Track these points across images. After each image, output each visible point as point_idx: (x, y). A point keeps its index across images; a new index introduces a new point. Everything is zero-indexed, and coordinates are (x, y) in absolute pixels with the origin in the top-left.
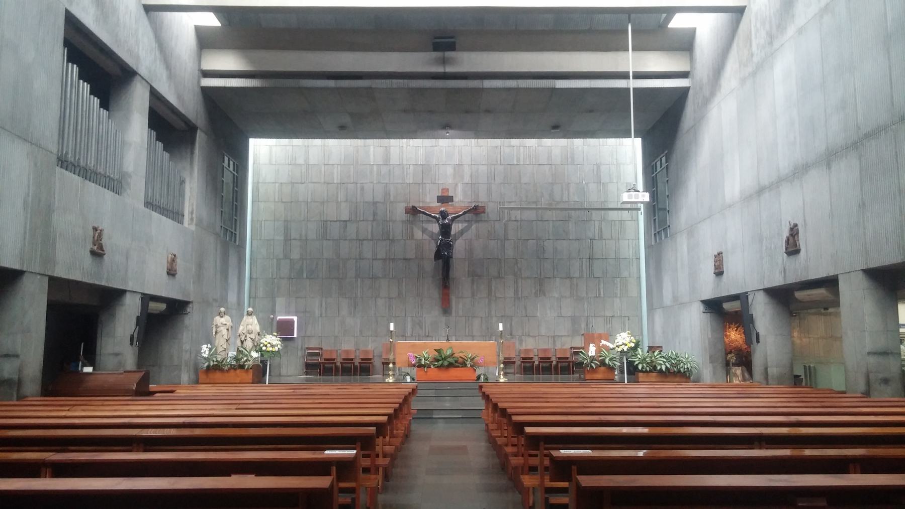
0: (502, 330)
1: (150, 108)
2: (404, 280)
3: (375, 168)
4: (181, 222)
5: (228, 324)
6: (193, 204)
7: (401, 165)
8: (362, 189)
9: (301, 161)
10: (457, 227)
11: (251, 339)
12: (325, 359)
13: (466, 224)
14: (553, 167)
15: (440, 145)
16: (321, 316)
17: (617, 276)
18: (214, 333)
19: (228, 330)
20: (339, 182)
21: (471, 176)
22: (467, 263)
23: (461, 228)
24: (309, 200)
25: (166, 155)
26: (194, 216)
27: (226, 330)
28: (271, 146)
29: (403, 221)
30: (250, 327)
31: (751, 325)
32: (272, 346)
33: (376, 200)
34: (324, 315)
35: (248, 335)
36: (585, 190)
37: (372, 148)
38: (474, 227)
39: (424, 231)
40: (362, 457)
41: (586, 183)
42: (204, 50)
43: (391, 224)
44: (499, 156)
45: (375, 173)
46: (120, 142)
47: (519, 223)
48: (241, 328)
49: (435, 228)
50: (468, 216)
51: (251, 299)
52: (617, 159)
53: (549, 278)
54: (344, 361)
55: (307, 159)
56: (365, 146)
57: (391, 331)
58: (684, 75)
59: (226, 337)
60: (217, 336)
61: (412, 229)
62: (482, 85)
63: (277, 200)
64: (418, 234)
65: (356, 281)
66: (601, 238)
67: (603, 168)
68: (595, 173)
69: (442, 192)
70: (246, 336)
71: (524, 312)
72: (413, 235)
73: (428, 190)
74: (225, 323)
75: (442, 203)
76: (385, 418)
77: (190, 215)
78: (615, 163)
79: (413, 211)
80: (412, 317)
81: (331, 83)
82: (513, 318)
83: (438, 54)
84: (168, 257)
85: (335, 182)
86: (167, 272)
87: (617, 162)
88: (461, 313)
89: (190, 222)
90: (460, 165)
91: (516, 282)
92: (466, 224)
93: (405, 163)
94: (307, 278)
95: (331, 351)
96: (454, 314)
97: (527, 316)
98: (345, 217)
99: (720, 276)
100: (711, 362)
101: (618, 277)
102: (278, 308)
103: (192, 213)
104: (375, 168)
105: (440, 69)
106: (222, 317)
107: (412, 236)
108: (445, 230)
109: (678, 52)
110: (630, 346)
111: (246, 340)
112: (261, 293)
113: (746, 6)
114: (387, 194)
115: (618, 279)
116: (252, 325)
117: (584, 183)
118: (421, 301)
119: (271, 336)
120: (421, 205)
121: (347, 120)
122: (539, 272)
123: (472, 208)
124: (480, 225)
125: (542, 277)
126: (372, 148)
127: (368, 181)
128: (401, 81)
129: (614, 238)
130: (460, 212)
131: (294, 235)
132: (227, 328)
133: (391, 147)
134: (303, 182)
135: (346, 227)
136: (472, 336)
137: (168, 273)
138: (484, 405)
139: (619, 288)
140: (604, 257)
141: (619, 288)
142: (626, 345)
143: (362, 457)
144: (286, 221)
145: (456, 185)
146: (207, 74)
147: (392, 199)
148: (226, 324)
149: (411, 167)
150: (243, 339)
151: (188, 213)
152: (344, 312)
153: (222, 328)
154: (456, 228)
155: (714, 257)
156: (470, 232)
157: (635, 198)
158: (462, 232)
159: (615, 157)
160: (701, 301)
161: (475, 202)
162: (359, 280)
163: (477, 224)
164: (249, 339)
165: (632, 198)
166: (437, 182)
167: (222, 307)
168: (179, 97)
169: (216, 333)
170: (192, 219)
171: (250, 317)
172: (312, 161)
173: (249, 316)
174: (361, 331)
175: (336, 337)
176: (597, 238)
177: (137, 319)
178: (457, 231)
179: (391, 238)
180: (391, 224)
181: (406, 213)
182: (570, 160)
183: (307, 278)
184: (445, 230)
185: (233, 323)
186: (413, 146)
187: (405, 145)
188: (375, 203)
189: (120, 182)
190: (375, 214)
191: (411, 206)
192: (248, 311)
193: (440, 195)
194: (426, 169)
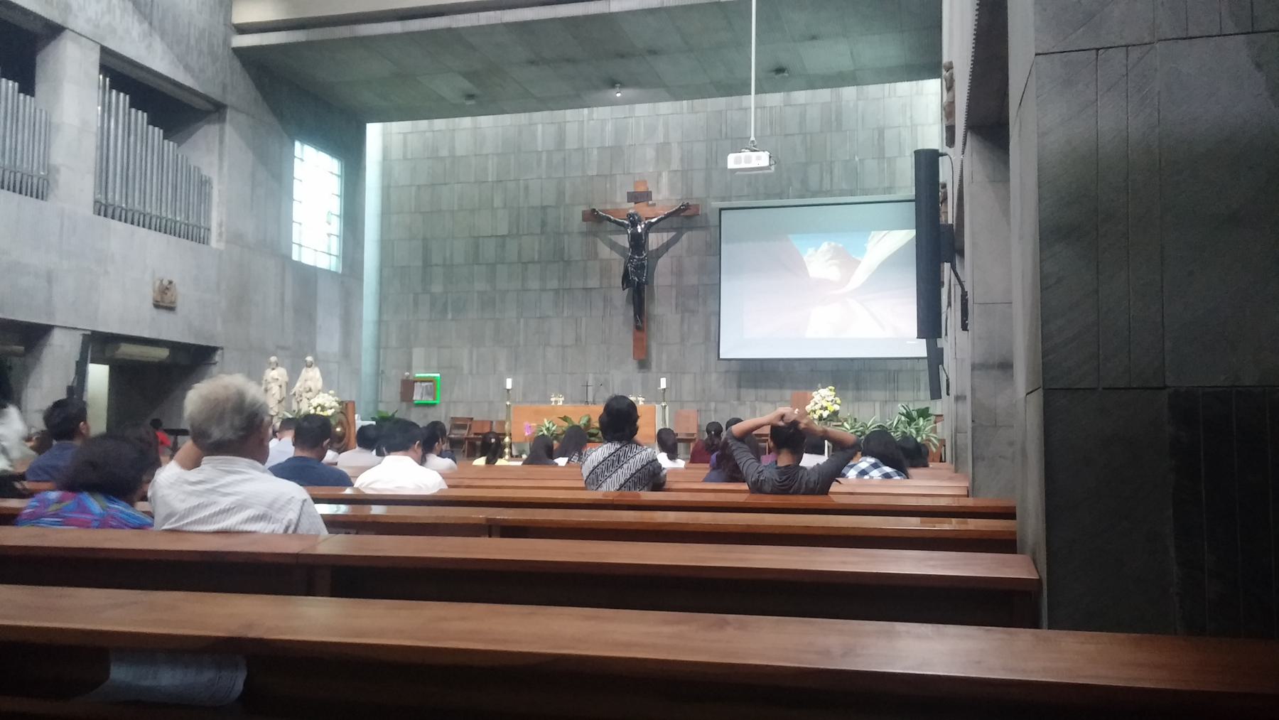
0: (665, 387)
2: (584, 319)
3: (544, 157)
4: (204, 240)
5: (280, 378)
7: (581, 150)
8: (527, 188)
9: (444, 152)
12: (475, 434)
13: (674, 234)
15: (636, 115)
16: (471, 373)
19: (280, 386)
20: (495, 179)
21: (682, 160)
22: (674, 294)
23: (665, 240)
24: (456, 208)
26: (223, 229)
27: (278, 387)
28: (405, 134)
29: (582, 233)
31: (940, 366)
32: (323, 408)
33: (545, 204)
34: (474, 372)
36: (858, 171)
37: (540, 127)
38: (685, 237)
39: (613, 246)
41: (860, 160)
43: (566, 237)
44: (724, 127)
45: (544, 164)
46: (43, 125)
48: (298, 384)
49: (624, 241)
50: (675, 221)
51: (382, 351)
52: (911, 117)
54: (476, 436)
55: (452, 149)
56: (531, 124)
57: (508, 390)
59: (278, 397)
61: (595, 245)
62: (609, 8)
63: (413, 210)
64: (605, 251)
65: (518, 322)
67: (888, 134)
68: (876, 142)
72: (596, 254)
73: (618, 184)
74: (276, 377)
75: (636, 203)
79: (594, 217)
80: (595, 373)
81: (396, 27)
84: (154, 283)
85: (490, 180)
87: (911, 121)
88: (664, 368)
90: (666, 144)
91: (605, 307)
92: (674, 234)
93: (585, 145)
94: (452, 320)
95: (483, 422)
96: (654, 364)
98: (503, 230)
102: (415, 363)
104: (544, 157)
106: (273, 369)
107: (594, 255)
108: (638, 243)
110: (832, 410)
111: (301, 400)
112: (393, 342)
114: (561, 193)
117: (857, 159)
119: (326, 395)
120: (608, 207)
124: (694, 233)
126: (540, 127)
131: (436, 259)
135: (503, 246)
136: (680, 401)
142: (826, 409)
144: (425, 239)
145: (660, 175)
146: (243, 29)
147: (567, 200)
148: (277, 379)
149: (595, 152)
152: (502, 367)
153: (273, 385)
154: (654, 240)
156: (678, 245)
157: (746, 162)
158: (666, 247)
159: (908, 114)
162: (522, 320)
163: (690, 232)
165: (740, 163)
166: (631, 171)
167: (273, 355)
168: (182, 60)
170: (220, 235)
171: (309, 369)
172: (460, 151)
174: (524, 395)
175: (491, 403)
177: (77, 365)
178: (661, 244)
181: (584, 220)
182: (834, 124)
183: (452, 320)
184: (638, 243)
186: (597, 120)
187: (585, 119)
188: (544, 208)
189: (46, 180)
190: (544, 224)
194: (616, 152)
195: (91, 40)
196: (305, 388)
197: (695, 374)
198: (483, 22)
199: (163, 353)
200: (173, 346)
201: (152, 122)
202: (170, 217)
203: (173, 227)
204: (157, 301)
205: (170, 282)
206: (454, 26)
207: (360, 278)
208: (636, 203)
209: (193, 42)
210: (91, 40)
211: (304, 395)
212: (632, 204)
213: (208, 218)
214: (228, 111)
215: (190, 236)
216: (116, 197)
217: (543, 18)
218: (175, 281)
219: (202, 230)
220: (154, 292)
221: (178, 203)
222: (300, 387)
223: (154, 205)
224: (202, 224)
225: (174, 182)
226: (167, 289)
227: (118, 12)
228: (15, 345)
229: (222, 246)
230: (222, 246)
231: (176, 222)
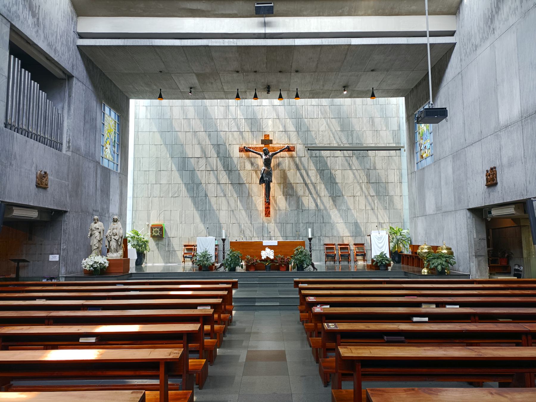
1: (11, 43)
4: (60, 150)
5: (100, 228)
6: (70, 136)
10: (275, 161)
11: (115, 239)
14: (342, 119)
15: (263, 105)
17: (387, 195)
18: (89, 235)
19: (100, 232)
25: (43, 95)
30: (115, 231)
35: (113, 237)
40: (278, 242)
42: (80, 17)
47: (318, 158)
53: (339, 196)
58: (452, 34)
59: (98, 238)
60: (92, 238)
62: (295, 43)
66: (375, 169)
69: (265, 137)
70: (111, 238)
71: (322, 219)
74: (97, 227)
76: (219, 300)
77: (67, 144)
78: (385, 117)
82: (314, 224)
83: (261, 19)
84: (37, 173)
86: (37, 186)
89: (67, 149)
97: (324, 223)
99: (492, 188)
100: (477, 256)
101: (387, 196)
103: (69, 142)
105: (262, 31)
109: (243, 288)
111: (111, 240)
113: (456, 31)
115: (387, 197)
116: (117, 229)
118: (251, 212)
120: (250, 146)
121: (194, 81)
122: (332, 193)
123: (285, 148)
125: (334, 195)
127: (214, 130)
128: (232, 40)
129: (384, 168)
130: (277, 150)
132: (99, 231)
133: (230, 107)
134: (169, 131)
137: (38, 186)
138: (299, 303)
139: (388, 203)
140: (377, 182)
141: (388, 203)
143: (278, 242)
146: (82, 36)
148: (98, 229)
150: (109, 240)
151: (65, 142)
155: (486, 172)
159: (384, 113)
160: (467, 209)
161: (287, 144)
164: (113, 240)
169: (91, 235)
170: (69, 147)
171: (115, 223)
173: (115, 222)
176: (372, 168)
179: (229, 169)
180: (230, 159)
185: (104, 227)
191: (243, 146)
192: (114, 219)
193: (263, 139)
195: (5, 18)
196: (113, 233)
197: (292, 223)
198: (226, 44)
199: (34, 214)
200: (41, 210)
201: (33, 78)
202: (42, 135)
203: (43, 141)
204: (38, 184)
205: (45, 173)
206: (210, 44)
207: (126, 176)
208: (265, 145)
209: (59, 37)
210: (5, 18)
211: (113, 237)
212: (263, 145)
213: (61, 138)
214: (75, 81)
215: (52, 146)
216: (13, 120)
217: (259, 45)
218: (48, 172)
219: (58, 144)
220: (37, 177)
221: (47, 128)
222: (110, 233)
223: (34, 126)
224: (59, 141)
225: (45, 115)
226: (44, 177)
227: (21, 6)
228: (309, 323)
229: (69, 154)
230: (69, 154)
231: (45, 138)
